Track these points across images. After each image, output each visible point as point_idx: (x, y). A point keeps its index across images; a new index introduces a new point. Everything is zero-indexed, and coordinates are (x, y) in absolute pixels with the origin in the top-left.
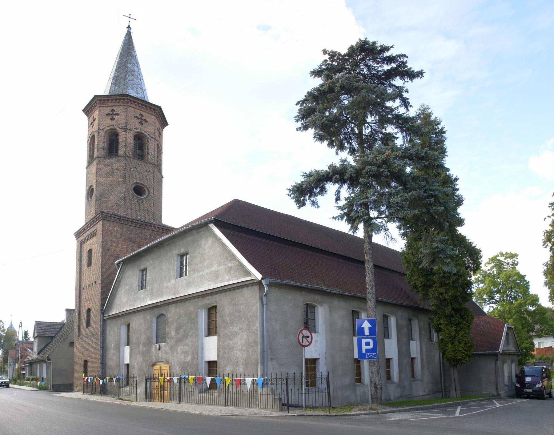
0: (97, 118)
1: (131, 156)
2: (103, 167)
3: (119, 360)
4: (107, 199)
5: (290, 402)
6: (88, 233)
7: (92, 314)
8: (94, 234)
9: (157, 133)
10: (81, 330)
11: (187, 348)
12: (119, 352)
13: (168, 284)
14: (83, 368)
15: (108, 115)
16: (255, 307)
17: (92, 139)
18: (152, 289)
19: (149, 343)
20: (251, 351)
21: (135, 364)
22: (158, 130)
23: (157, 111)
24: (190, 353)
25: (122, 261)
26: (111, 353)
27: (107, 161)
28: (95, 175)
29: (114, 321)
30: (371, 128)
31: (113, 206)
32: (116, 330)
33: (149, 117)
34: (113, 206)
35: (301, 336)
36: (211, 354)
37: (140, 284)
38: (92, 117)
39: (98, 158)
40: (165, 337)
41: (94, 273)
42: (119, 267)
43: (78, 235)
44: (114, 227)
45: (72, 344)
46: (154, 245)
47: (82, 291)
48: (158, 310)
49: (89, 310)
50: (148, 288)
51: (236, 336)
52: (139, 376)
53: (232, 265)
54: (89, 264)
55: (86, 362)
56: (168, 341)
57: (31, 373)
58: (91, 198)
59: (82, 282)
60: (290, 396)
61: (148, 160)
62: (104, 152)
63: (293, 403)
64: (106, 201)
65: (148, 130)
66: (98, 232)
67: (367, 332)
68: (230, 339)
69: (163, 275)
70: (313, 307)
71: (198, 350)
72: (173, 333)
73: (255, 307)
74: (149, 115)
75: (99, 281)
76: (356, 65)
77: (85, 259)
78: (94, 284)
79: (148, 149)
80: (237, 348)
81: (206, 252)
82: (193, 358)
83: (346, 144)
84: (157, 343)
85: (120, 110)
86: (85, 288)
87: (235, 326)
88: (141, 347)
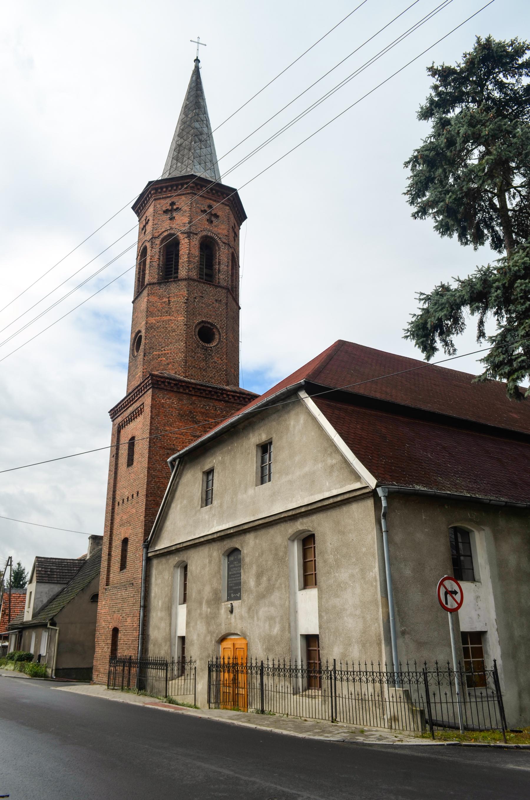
0: (151, 219)
1: (195, 277)
2: (156, 298)
3: (170, 629)
4: (160, 353)
5: (434, 718)
6: (131, 409)
7: (131, 548)
8: (139, 412)
9: (232, 235)
10: (111, 575)
11: (272, 610)
12: (170, 615)
13: (245, 496)
14: (110, 641)
15: (166, 212)
16: (370, 537)
17: (143, 253)
18: (221, 506)
19: (216, 601)
20: (368, 617)
21: (195, 637)
22: (233, 228)
23: (231, 200)
24: (278, 620)
25: (179, 457)
26: (156, 616)
27: (161, 290)
28: (144, 314)
29: (164, 560)
30: (521, 195)
31: (168, 364)
32: (166, 575)
33: (219, 208)
34: (168, 364)
35: (442, 591)
36: (308, 623)
37: (204, 497)
38: (144, 217)
39: (150, 284)
40: (239, 590)
41: (136, 478)
42: (173, 466)
43: (114, 413)
44: (169, 399)
45: (95, 598)
46: (223, 429)
47: (117, 507)
48: (229, 543)
49: (125, 541)
50: (215, 502)
51: (346, 589)
52: (201, 659)
53: (334, 461)
54: (130, 462)
55: (116, 631)
56: (244, 596)
57: (18, 646)
58: (137, 351)
59: (118, 492)
60: (432, 705)
61: (219, 282)
62: (158, 274)
63: (439, 718)
64: (159, 356)
65: (220, 231)
66: (145, 408)
68: (337, 596)
69: (237, 481)
70: (466, 535)
71: (290, 615)
72: (252, 583)
73: (370, 537)
75: (143, 492)
76: (481, 84)
77: (122, 452)
78: (135, 496)
79: (219, 263)
80: (348, 612)
81: (297, 439)
82: (283, 630)
83: (486, 231)
84: (228, 600)
86: (121, 502)
87: (343, 570)
88: (204, 607)
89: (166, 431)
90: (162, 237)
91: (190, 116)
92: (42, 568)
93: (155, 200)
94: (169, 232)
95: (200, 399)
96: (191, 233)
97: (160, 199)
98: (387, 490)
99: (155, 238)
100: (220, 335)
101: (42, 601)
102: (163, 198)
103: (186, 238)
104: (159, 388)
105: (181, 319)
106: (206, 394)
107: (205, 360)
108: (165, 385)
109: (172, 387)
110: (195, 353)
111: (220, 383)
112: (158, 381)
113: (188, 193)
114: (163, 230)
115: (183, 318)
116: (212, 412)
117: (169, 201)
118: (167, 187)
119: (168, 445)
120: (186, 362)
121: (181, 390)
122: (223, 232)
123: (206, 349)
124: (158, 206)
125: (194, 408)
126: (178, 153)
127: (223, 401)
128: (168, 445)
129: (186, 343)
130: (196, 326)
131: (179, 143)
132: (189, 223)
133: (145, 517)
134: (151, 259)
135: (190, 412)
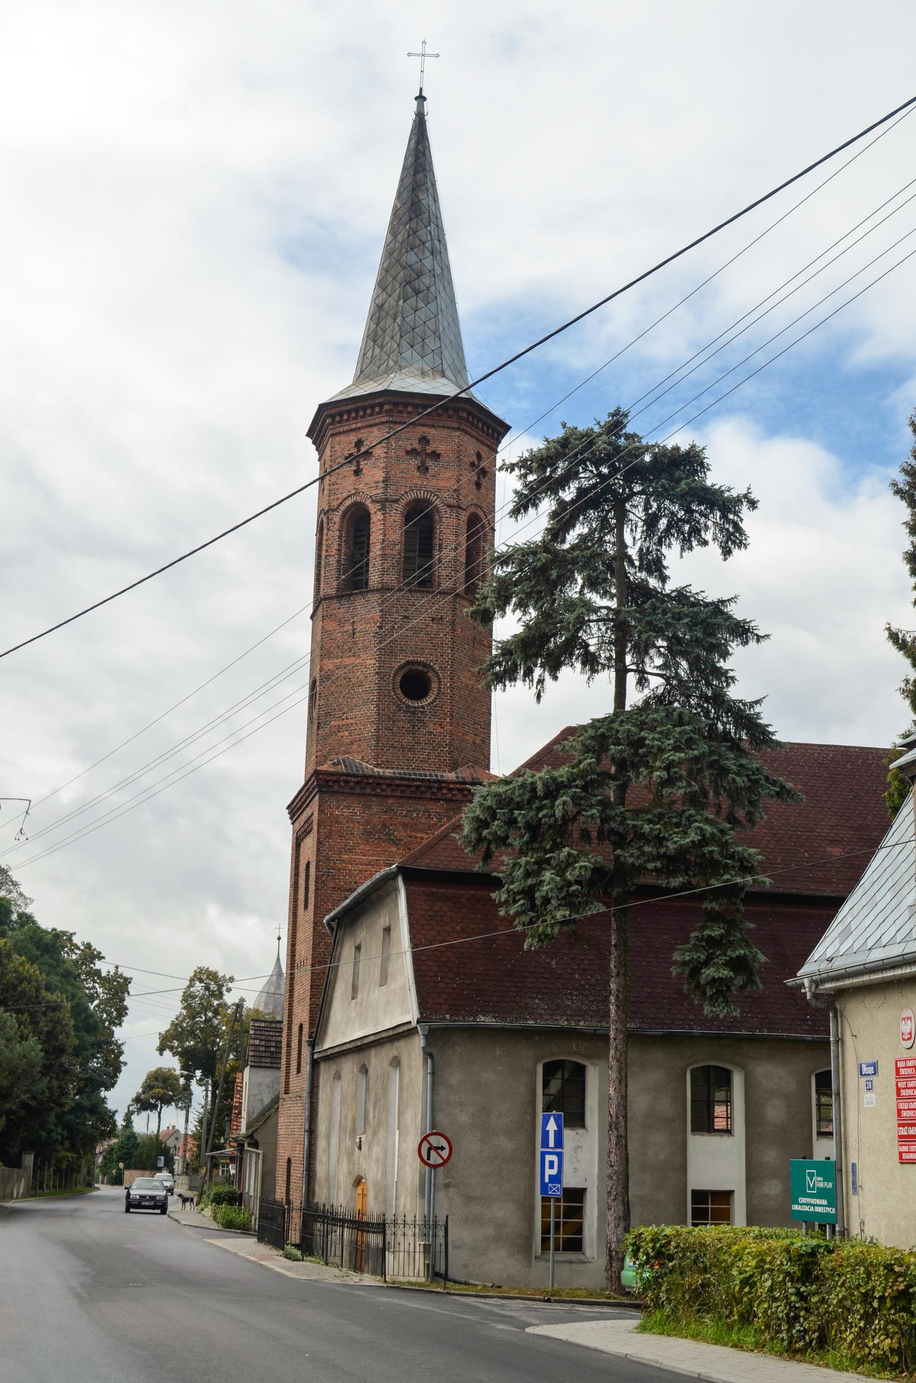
2: (334, 625)
4: (341, 723)
34: (352, 743)
35: (425, 1146)
44: (348, 807)
55: (289, 1161)
64: (339, 729)
65: (442, 484)
67: (552, 1143)
74: (445, 432)
85: (373, 437)
89: (344, 861)
90: (342, 508)
91: (400, 238)
92: (261, 1040)
93: (332, 435)
94: (354, 499)
95: (401, 801)
96: (387, 500)
97: (340, 433)
98: (427, 1028)
99: (333, 510)
100: (440, 682)
101: (262, 1100)
102: (344, 432)
103: (379, 510)
104: (331, 792)
105: (370, 662)
106: (412, 792)
107: (412, 732)
108: (340, 786)
109: (352, 788)
110: (394, 722)
111: (439, 769)
112: (328, 781)
113: (383, 423)
114: (345, 495)
115: (373, 661)
116: (423, 820)
117: (353, 438)
118: (349, 412)
119: (345, 883)
120: (378, 739)
121: (368, 791)
122: (448, 485)
123: (414, 712)
124: (337, 447)
125: (391, 819)
126: (377, 325)
127: (443, 800)
128: (345, 883)
129: (378, 706)
130: (396, 674)
131: (379, 301)
132: (384, 481)
133: (310, 999)
134: (327, 551)
135: (384, 826)
